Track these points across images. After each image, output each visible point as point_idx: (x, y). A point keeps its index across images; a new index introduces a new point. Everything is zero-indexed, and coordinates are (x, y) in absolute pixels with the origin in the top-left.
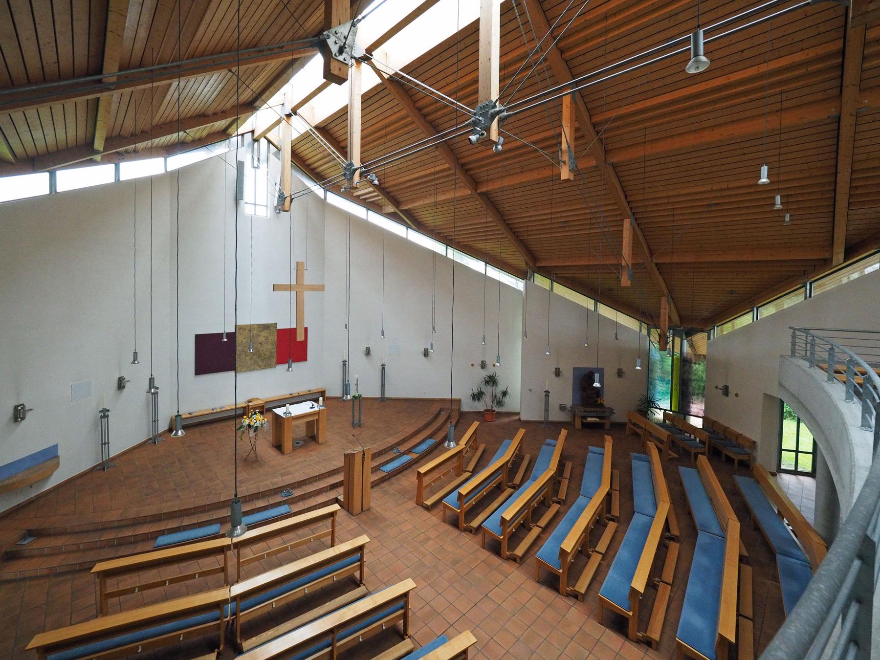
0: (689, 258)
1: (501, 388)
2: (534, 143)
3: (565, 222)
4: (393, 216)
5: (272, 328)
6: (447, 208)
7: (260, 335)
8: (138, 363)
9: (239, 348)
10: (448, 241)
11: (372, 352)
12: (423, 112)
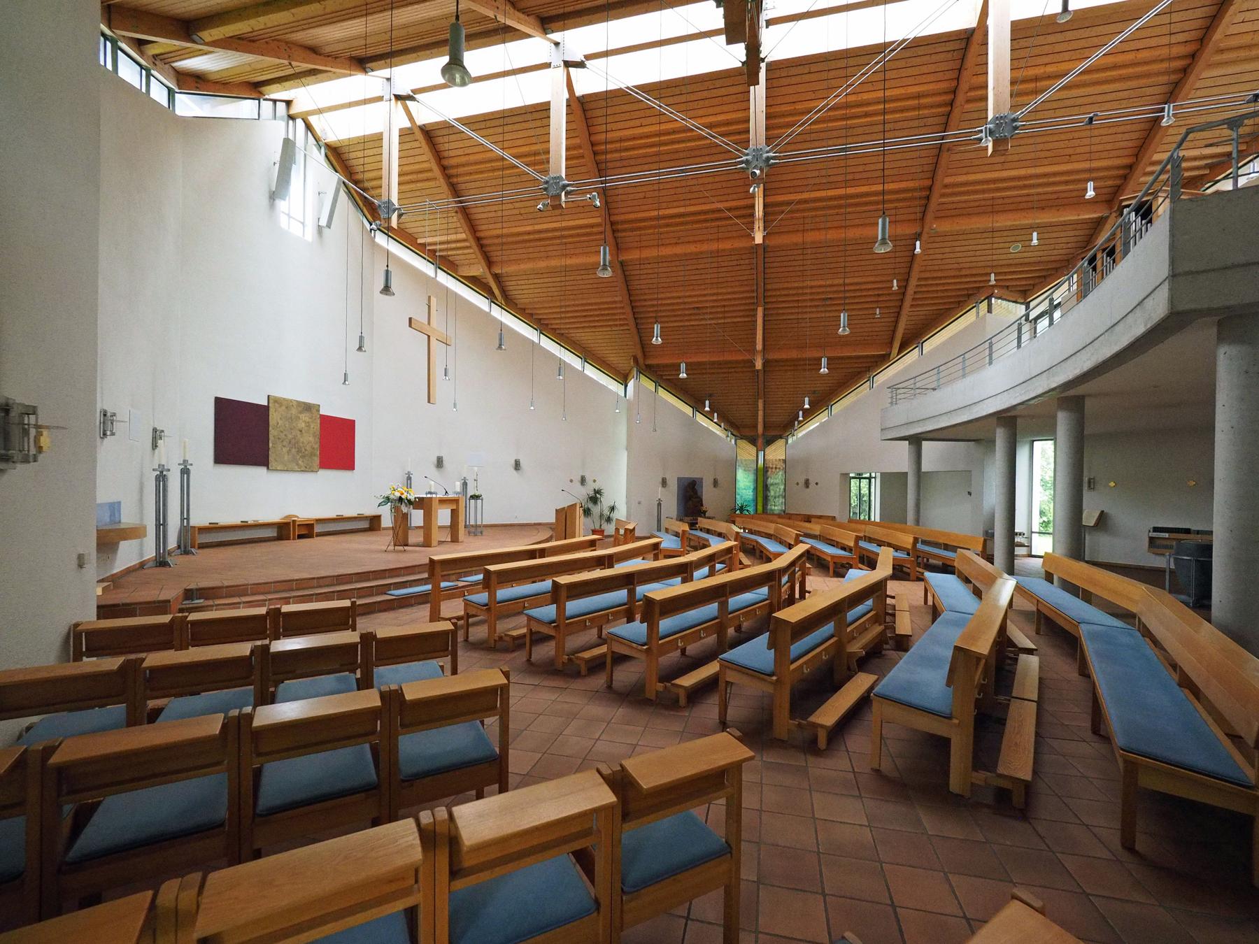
0: (794, 354)
1: (660, 492)
2: (729, 209)
3: (697, 308)
4: (475, 283)
5: (315, 411)
6: (546, 280)
7: (299, 418)
8: (113, 434)
9: (273, 433)
10: (542, 326)
11: (445, 463)
12: (596, 148)
